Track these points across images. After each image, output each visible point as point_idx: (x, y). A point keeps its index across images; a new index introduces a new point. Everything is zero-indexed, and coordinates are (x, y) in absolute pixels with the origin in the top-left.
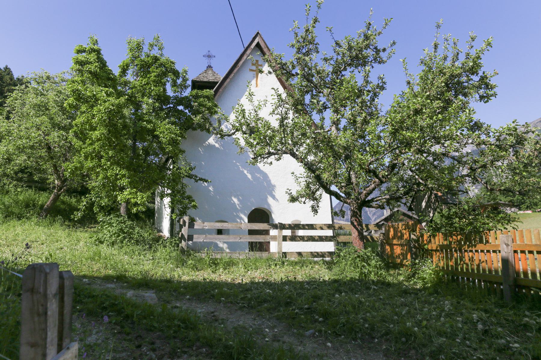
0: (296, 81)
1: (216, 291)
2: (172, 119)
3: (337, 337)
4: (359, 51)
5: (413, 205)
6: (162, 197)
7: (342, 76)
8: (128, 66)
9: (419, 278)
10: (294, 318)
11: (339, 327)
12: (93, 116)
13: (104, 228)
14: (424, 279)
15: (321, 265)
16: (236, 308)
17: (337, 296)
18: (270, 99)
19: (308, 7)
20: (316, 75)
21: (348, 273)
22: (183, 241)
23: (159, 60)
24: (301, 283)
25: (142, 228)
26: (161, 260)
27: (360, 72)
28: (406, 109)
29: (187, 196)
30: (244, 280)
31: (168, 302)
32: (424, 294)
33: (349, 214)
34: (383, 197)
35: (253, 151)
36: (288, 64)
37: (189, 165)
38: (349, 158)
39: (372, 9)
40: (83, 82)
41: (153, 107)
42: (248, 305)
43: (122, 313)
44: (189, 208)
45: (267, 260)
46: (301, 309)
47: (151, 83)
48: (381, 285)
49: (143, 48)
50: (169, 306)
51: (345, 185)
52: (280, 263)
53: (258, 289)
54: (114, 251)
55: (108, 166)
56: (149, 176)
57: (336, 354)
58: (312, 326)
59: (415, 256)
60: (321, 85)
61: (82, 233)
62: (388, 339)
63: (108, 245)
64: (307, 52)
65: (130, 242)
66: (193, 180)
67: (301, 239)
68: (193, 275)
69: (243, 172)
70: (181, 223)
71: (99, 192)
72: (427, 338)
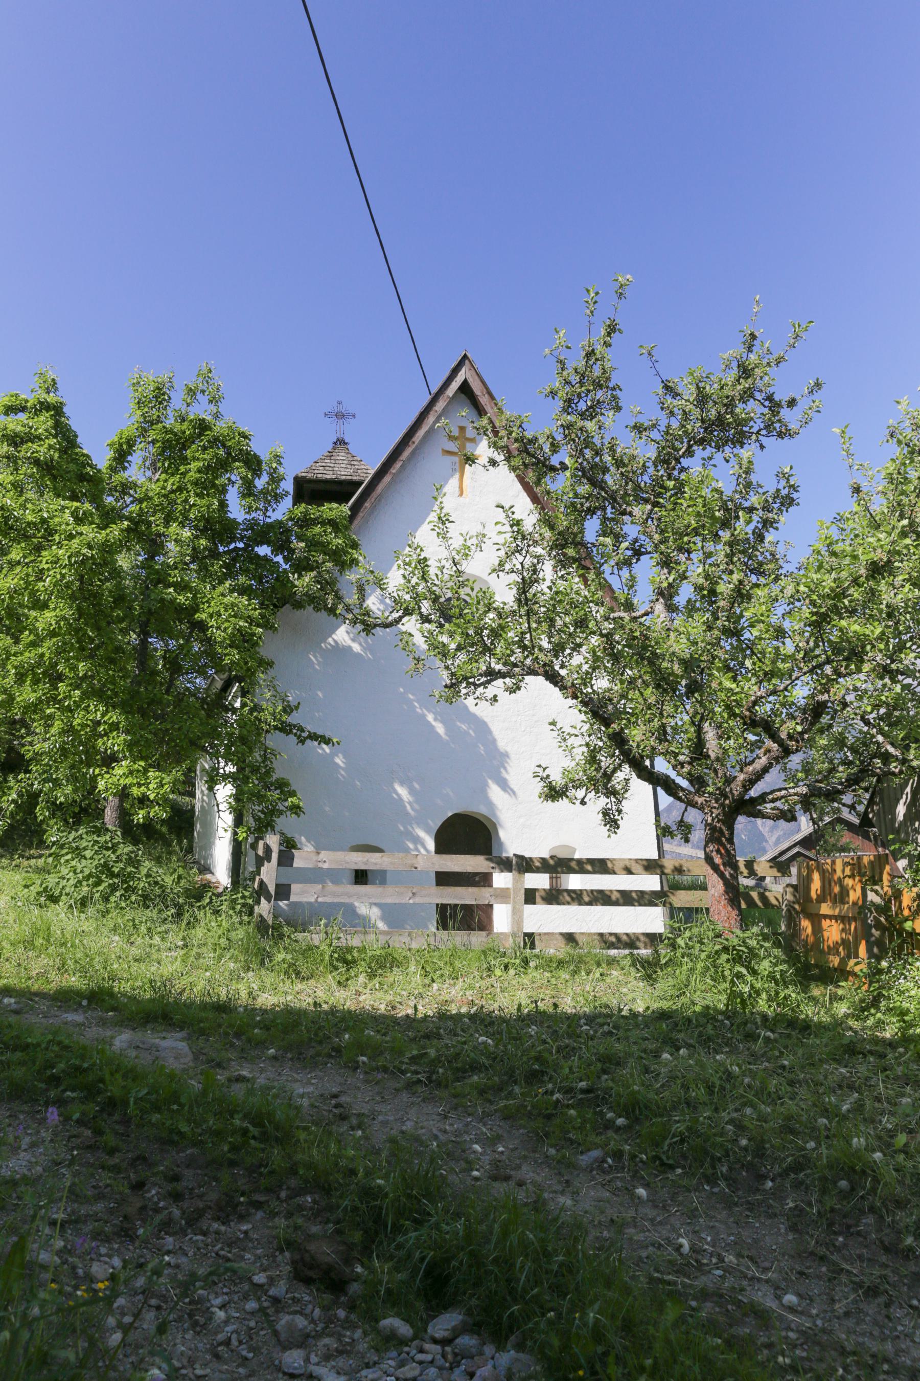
0: (560, 484)
1: (347, 1036)
2: (242, 579)
3: (665, 1172)
4: (725, 405)
5: (873, 811)
6: (213, 780)
7: (683, 470)
8: (131, 443)
9: (889, 1010)
10: (549, 1117)
11: (670, 1144)
12: (40, 575)
13: (62, 861)
14: (903, 1013)
15: (627, 968)
16: (398, 1086)
17: (666, 1056)
18: (492, 532)
19: (592, 295)
20: (613, 469)
21: (698, 993)
22: (262, 899)
23: (210, 429)
24: (572, 1020)
25: (158, 860)
26: (204, 950)
27: (727, 461)
28: (847, 560)
29: (277, 780)
30: (420, 1007)
31: (219, 1065)
32: (902, 1055)
33: (699, 835)
34: (792, 791)
35: (447, 668)
36: (541, 441)
37: (284, 701)
38: (697, 691)
39: (758, 297)
40: (18, 488)
41: (194, 549)
42: (429, 1079)
43: (99, 1092)
44: (281, 813)
45: (484, 952)
46: (569, 1091)
47: (189, 487)
48: (785, 1028)
49: (170, 398)
50: (221, 1077)
51: (688, 759)
52: (518, 961)
53: (456, 1035)
54: (86, 922)
55: (75, 702)
56: (180, 729)
57: (658, 1219)
58: (598, 1140)
59: (878, 951)
60: (626, 494)
61: (5, 872)
62: (802, 1183)
63: (71, 906)
64: (589, 408)
65: (126, 900)
66: (292, 739)
67: (573, 899)
68: (286, 993)
69: (424, 716)
70: (260, 852)
71: (51, 766)
72: (908, 1181)
